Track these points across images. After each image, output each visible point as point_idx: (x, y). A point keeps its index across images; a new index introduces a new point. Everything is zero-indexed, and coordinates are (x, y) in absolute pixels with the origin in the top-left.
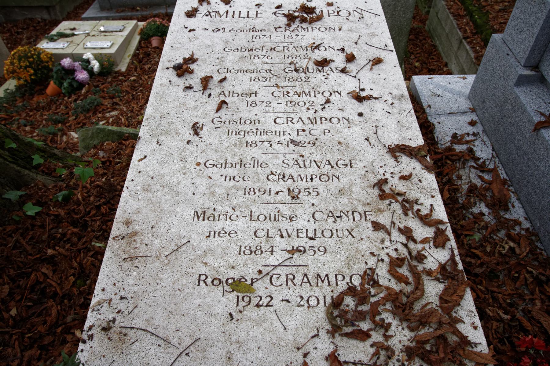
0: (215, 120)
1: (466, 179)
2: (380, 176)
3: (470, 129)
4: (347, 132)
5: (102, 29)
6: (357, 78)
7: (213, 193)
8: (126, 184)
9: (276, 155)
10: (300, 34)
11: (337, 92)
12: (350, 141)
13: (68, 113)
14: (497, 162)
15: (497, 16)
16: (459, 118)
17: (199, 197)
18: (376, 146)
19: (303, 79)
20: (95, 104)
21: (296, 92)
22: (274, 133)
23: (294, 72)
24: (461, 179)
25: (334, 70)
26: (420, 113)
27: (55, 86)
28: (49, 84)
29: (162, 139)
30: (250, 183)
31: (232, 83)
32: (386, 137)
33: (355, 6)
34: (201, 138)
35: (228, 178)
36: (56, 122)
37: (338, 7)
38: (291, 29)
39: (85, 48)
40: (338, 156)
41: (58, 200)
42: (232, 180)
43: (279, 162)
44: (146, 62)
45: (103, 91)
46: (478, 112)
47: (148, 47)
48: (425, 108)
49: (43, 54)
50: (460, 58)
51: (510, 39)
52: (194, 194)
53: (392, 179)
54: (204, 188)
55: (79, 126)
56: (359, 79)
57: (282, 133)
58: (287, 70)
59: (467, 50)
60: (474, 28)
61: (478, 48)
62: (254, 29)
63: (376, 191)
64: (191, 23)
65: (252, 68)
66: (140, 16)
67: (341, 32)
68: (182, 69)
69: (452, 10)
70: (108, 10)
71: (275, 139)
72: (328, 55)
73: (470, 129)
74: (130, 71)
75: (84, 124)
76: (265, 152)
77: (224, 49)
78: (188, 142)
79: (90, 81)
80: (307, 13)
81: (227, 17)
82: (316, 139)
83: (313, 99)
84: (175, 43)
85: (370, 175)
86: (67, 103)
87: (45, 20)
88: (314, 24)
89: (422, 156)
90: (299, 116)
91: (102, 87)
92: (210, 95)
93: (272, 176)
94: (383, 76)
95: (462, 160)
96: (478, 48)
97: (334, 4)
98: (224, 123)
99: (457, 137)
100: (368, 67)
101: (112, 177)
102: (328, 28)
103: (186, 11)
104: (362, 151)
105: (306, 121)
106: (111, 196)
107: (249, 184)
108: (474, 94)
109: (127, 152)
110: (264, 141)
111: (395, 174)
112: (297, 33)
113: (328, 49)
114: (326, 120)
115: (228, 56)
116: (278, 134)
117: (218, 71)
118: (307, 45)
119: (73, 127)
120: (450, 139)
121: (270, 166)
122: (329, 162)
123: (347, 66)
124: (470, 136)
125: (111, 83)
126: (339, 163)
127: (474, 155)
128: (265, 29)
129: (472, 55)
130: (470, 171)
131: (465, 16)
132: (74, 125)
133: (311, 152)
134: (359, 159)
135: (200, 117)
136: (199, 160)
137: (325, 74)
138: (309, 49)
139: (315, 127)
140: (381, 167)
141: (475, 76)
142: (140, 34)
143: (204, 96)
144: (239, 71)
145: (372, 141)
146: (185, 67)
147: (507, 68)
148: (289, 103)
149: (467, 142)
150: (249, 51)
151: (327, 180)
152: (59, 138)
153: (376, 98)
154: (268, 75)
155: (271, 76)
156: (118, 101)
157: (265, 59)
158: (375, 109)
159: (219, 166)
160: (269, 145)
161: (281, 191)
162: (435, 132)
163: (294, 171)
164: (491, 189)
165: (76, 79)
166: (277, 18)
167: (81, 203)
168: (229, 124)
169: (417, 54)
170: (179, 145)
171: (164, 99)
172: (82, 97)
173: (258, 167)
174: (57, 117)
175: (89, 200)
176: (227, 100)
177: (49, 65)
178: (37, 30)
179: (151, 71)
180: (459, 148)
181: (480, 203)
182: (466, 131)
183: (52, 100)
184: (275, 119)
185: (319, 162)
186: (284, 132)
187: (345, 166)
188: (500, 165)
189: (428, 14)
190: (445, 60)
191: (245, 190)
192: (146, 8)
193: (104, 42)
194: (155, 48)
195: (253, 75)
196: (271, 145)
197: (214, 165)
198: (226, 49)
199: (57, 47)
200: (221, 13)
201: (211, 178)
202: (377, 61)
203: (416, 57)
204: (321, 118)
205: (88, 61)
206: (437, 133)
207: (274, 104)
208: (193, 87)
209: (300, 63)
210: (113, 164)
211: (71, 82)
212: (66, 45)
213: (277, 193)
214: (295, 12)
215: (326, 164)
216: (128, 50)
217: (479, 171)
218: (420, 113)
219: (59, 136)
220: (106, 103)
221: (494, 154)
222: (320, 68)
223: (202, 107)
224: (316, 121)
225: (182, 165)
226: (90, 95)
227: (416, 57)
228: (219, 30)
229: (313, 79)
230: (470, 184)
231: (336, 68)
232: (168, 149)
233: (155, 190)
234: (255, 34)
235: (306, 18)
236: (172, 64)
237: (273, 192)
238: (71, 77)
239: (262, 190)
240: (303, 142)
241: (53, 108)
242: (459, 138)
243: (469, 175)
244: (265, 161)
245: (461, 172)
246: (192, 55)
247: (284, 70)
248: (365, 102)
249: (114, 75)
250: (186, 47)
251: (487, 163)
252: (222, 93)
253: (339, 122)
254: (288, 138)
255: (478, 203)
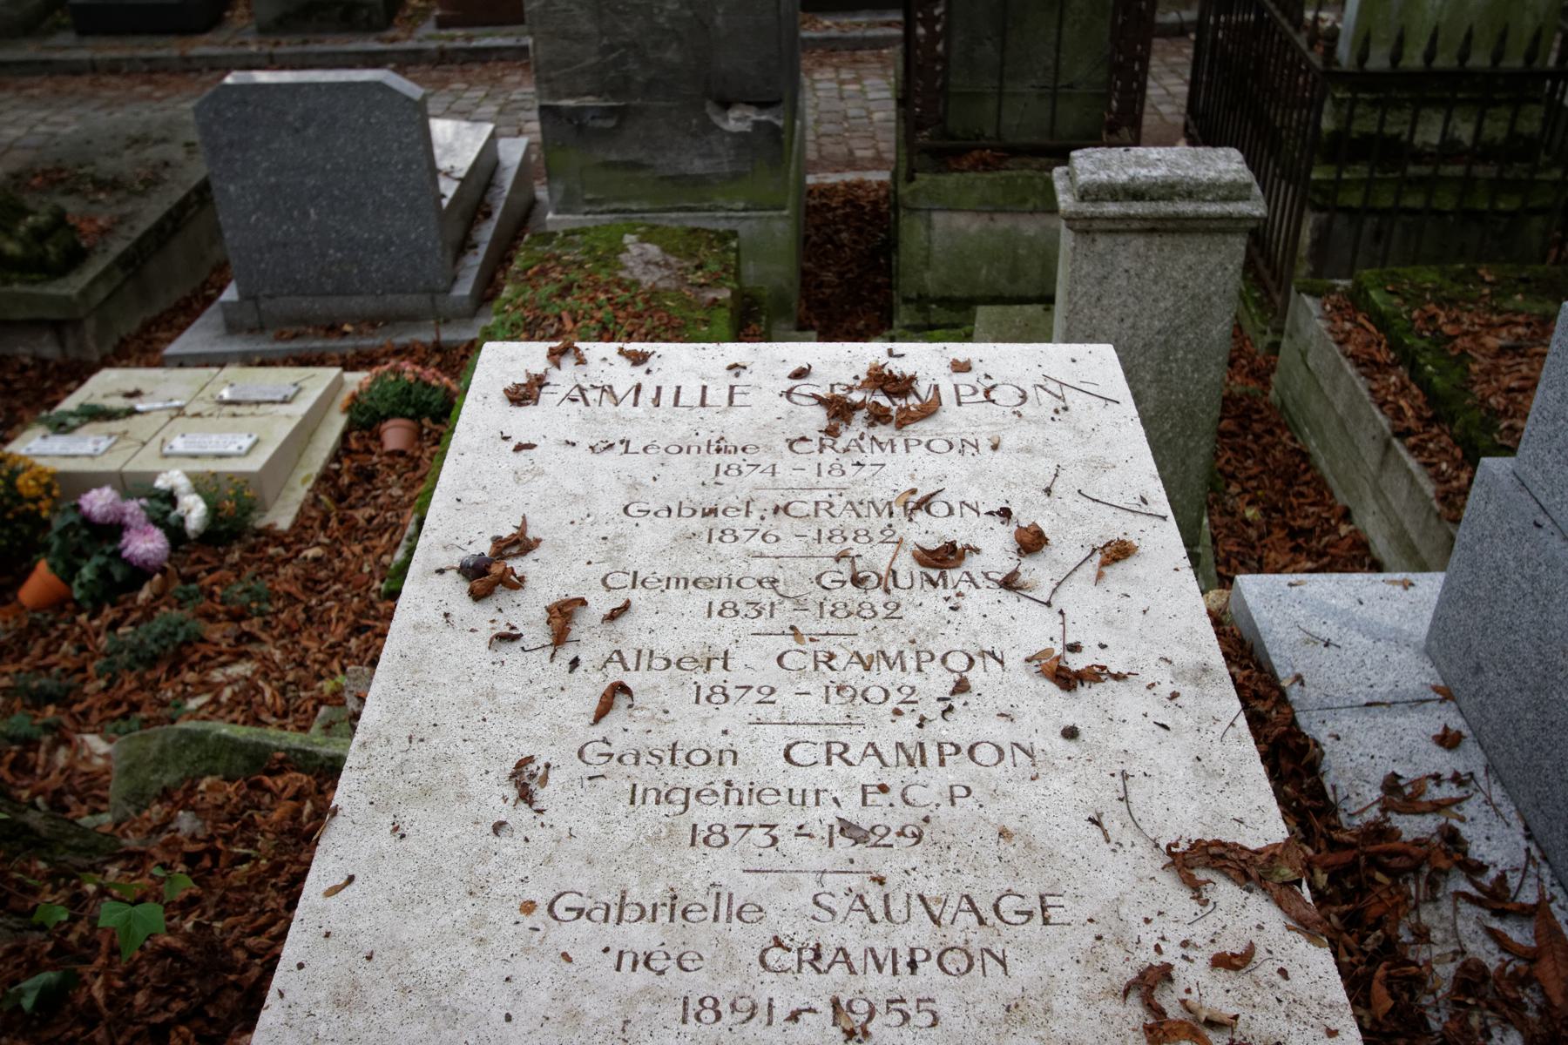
0: (588, 750)
1: (1445, 942)
2: (1146, 957)
3: (1445, 763)
4: (1028, 794)
5: (226, 394)
6: (1056, 607)
7: (575, 1015)
8: (277, 982)
9: (789, 875)
10: (868, 462)
11: (992, 654)
12: (1038, 828)
13: (83, 669)
14: (1547, 879)
15: (1496, 367)
16: (1400, 720)
17: (525, 1029)
18: (1127, 847)
19: (880, 609)
20: (180, 639)
21: (857, 654)
22: (784, 797)
23: (849, 585)
24: (1429, 942)
25: (980, 580)
26: (1269, 703)
27: (53, 579)
28: (30, 570)
29: (413, 815)
30: (702, 977)
31: (648, 623)
32: (1159, 814)
33: (1040, 371)
34: (540, 811)
35: (627, 960)
36: (39, 699)
37: (987, 376)
38: (841, 443)
39: (166, 456)
40: (998, 881)
41: (19, 1008)
42: (640, 966)
43: (802, 901)
44: (362, 498)
45: (211, 595)
46: (1464, 703)
47: (370, 452)
48: (1285, 684)
49: (26, 475)
50: (1390, 496)
51: (1538, 476)
52: (508, 1018)
53: (1185, 964)
54: (544, 997)
55: (117, 713)
56: (1061, 612)
57: (811, 799)
58: (826, 581)
59: (1409, 471)
60: (1426, 403)
61: (1444, 466)
62: (722, 445)
63: (1135, 1012)
64: (524, 422)
65: (715, 571)
66: (351, 352)
67: (998, 454)
68: (487, 576)
69: (1350, 348)
70: (251, 331)
71: (788, 820)
72: (957, 530)
73: (1445, 763)
74: (305, 528)
75: (135, 707)
76: (755, 863)
77: (626, 509)
78: (498, 828)
79: (170, 559)
80: (888, 394)
81: (635, 404)
82: (926, 820)
83: (912, 679)
84: (468, 488)
85: (1111, 950)
86: (84, 632)
87: (45, 361)
88: (911, 427)
89: (1285, 884)
90: (866, 736)
91: (208, 580)
92: (575, 663)
93: (778, 951)
94: (1139, 601)
95: (1426, 870)
96: (1444, 466)
97: (975, 365)
98: (620, 760)
99: (1399, 789)
100: (1090, 569)
101: (220, 916)
102: (956, 441)
103: (509, 384)
104: (1080, 862)
105: (889, 754)
106: (209, 988)
107: (698, 983)
108: (1443, 640)
109: (275, 816)
110: (750, 827)
111: (1196, 947)
112: (859, 457)
113: (957, 511)
114: (958, 750)
115: (636, 530)
116: (797, 799)
117: (604, 581)
118: (890, 496)
119: (95, 717)
120: (1377, 794)
121: (772, 915)
122: (971, 902)
123: (1021, 569)
124: (1445, 786)
125: (237, 569)
126: (1003, 905)
127: (1465, 853)
128: (759, 443)
129: (1430, 488)
130: (1456, 910)
131: (1395, 364)
132: (101, 710)
133: (908, 867)
134: (1070, 891)
135: (539, 740)
136: (531, 893)
137: (950, 592)
138: (897, 510)
139: (920, 778)
140: (1147, 921)
141: (1440, 577)
142: (348, 409)
143: (555, 665)
144: (673, 582)
145: (1113, 826)
146: (496, 569)
147: (1543, 568)
148: (833, 690)
149: (1438, 807)
150: (704, 515)
151: (964, 968)
152: (42, 756)
153: (1118, 677)
154: (766, 596)
155: (776, 598)
156: (256, 630)
157: (756, 544)
158: (1117, 715)
159: (598, 915)
160: (769, 841)
161: (810, 1010)
162: (1323, 768)
163: (849, 933)
164: (1537, 979)
165: (125, 554)
166: (796, 409)
167: (101, 1017)
168: (637, 763)
169: (1250, 478)
170: (467, 838)
171: (424, 676)
172: (135, 615)
173: (729, 920)
174: (44, 681)
175: (130, 1005)
176: (631, 680)
177: (39, 510)
178: (15, 393)
179: (374, 530)
180: (1412, 827)
181: (1504, 1031)
182: (1428, 768)
183: (34, 625)
184: (789, 747)
185: (938, 900)
186: (817, 792)
187: (1023, 918)
188: (1557, 891)
189: (1277, 354)
190: (1342, 499)
191: (685, 1003)
192: (374, 326)
193: (229, 437)
194: (392, 454)
195: (718, 597)
196: (775, 840)
197: (580, 912)
198: (631, 510)
199: (72, 451)
200: (619, 392)
201: (569, 960)
202: (1118, 552)
203: (1245, 491)
204: (940, 745)
205: (170, 498)
206: (1332, 774)
207: (785, 696)
208: (518, 637)
209: (867, 556)
210: (223, 861)
211: (108, 564)
212: (103, 445)
213: (794, 1017)
214: (850, 389)
215: (959, 910)
216: (304, 461)
217: (1487, 913)
218: (1269, 703)
219: (43, 748)
220: (217, 636)
221: (1534, 852)
222: (934, 574)
223: (544, 704)
224: (923, 755)
225: (472, 911)
226: (164, 609)
227: (1245, 491)
228: (611, 446)
229: (911, 609)
230: (1460, 960)
231: (986, 575)
232: (427, 853)
233: (376, 1000)
234: (725, 459)
235: (888, 409)
236: (456, 558)
237: (781, 1012)
238: (109, 549)
239: (743, 1004)
240: (880, 831)
241: (37, 650)
242: (1408, 790)
243: (1454, 924)
244: (754, 899)
245: (1427, 916)
246: (523, 528)
247: (819, 578)
248: (1083, 691)
249: (253, 540)
250: (503, 502)
251: (1513, 881)
252: (615, 657)
253: (1001, 760)
254: (829, 813)
255: (1496, 1032)
